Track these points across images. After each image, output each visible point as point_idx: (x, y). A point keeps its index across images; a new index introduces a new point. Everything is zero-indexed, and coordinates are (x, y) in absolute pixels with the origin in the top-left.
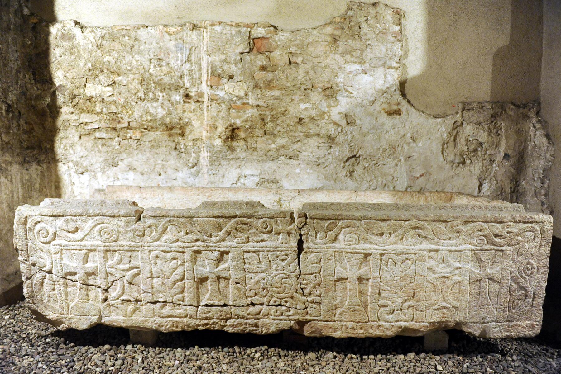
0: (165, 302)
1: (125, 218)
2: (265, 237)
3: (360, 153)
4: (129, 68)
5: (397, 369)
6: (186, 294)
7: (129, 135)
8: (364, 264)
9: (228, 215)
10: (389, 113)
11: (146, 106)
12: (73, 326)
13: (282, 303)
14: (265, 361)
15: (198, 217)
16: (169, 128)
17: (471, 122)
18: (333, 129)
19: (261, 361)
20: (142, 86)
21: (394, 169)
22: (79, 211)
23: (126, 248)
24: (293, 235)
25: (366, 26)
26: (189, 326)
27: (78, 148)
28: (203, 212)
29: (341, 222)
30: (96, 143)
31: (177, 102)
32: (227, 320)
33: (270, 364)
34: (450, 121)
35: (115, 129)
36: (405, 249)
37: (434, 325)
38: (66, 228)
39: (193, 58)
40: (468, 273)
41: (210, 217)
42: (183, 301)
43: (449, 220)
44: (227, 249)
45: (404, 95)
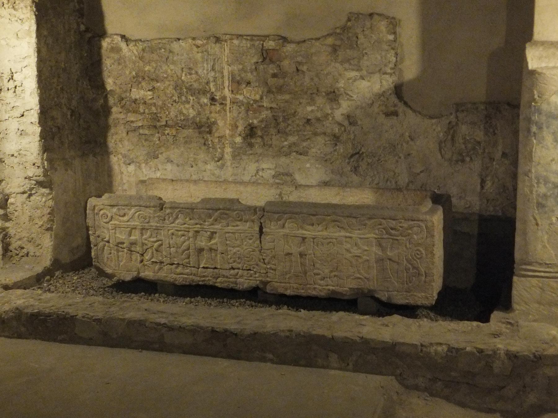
0: (178, 264)
1: (153, 208)
2: (238, 223)
3: (363, 150)
4: (165, 76)
11: (180, 108)
13: (251, 269)
16: (199, 126)
20: (176, 91)
22: (126, 203)
23: (154, 228)
25: (362, 37)
26: (193, 281)
27: (126, 143)
28: (200, 206)
35: (155, 127)
36: (328, 235)
38: (118, 214)
39: (217, 67)
42: (190, 264)
44: (215, 230)
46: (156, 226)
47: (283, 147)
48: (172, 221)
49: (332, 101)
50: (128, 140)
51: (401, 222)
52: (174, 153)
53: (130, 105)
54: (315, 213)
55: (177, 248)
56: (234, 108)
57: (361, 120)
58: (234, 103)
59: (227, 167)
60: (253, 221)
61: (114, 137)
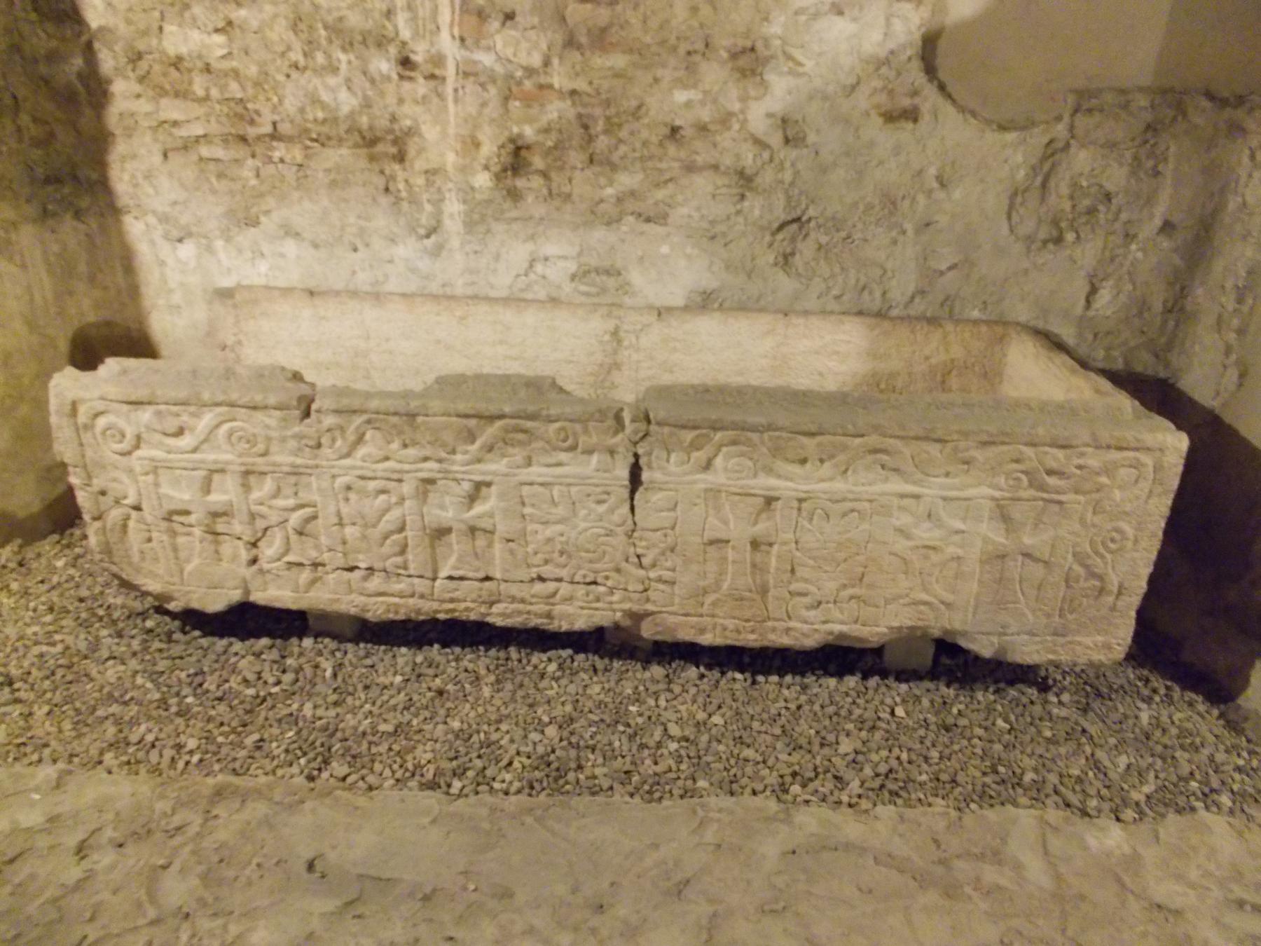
0: (370, 569)
1: (278, 413)
2: (563, 456)
3: (811, 212)
5: (817, 707)
6: (410, 557)
7: (277, 155)
8: (764, 516)
10: (890, 117)
12: (195, 605)
13: (599, 580)
14: (564, 682)
15: (427, 415)
16: (369, 141)
17: (1090, 143)
18: (750, 156)
19: (557, 680)
20: (296, 33)
22: (182, 394)
26: (418, 612)
28: (436, 405)
30: (202, 171)
31: (382, 76)
32: (492, 604)
33: (572, 689)
34: (1038, 138)
35: (243, 139)
38: (158, 427)
40: (979, 543)
41: (449, 415)
42: (406, 568)
44: (488, 478)
45: (930, 70)
46: (293, 466)
47: (602, 201)
48: (345, 451)
49: (744, 76)
50: (170, 175)
51: (1082, 455)
52: (302, 212)
53: (165, 75)
54: (813, 428)
55: (366, 526)
56: (467, 90)
57: (818, 131)
58: (466, 75)
59: (450, 250)
60: (612, 452)
61: (128, 166)
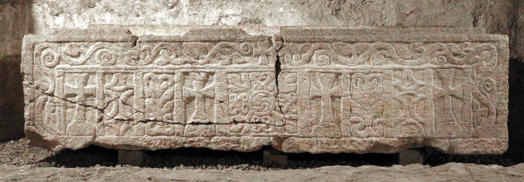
0: (155, 120)
1: (122, 43)
2: (247, 59)
6: (175, 113)
8: (335, 83)
9: (213, 39)
12: (69, 146)
15: (187, 42)
21: (382, 6)
23: (122, 71)
24: (271, 57)
26: (176, 143)
28: (192, 38)
29: (313, 45)
36: (372, 68)
37: (403, 141)
38: (70, 53)
41: (197, 41)
42: (172, 119)
43: (411, 41)
44: (213, 70)
